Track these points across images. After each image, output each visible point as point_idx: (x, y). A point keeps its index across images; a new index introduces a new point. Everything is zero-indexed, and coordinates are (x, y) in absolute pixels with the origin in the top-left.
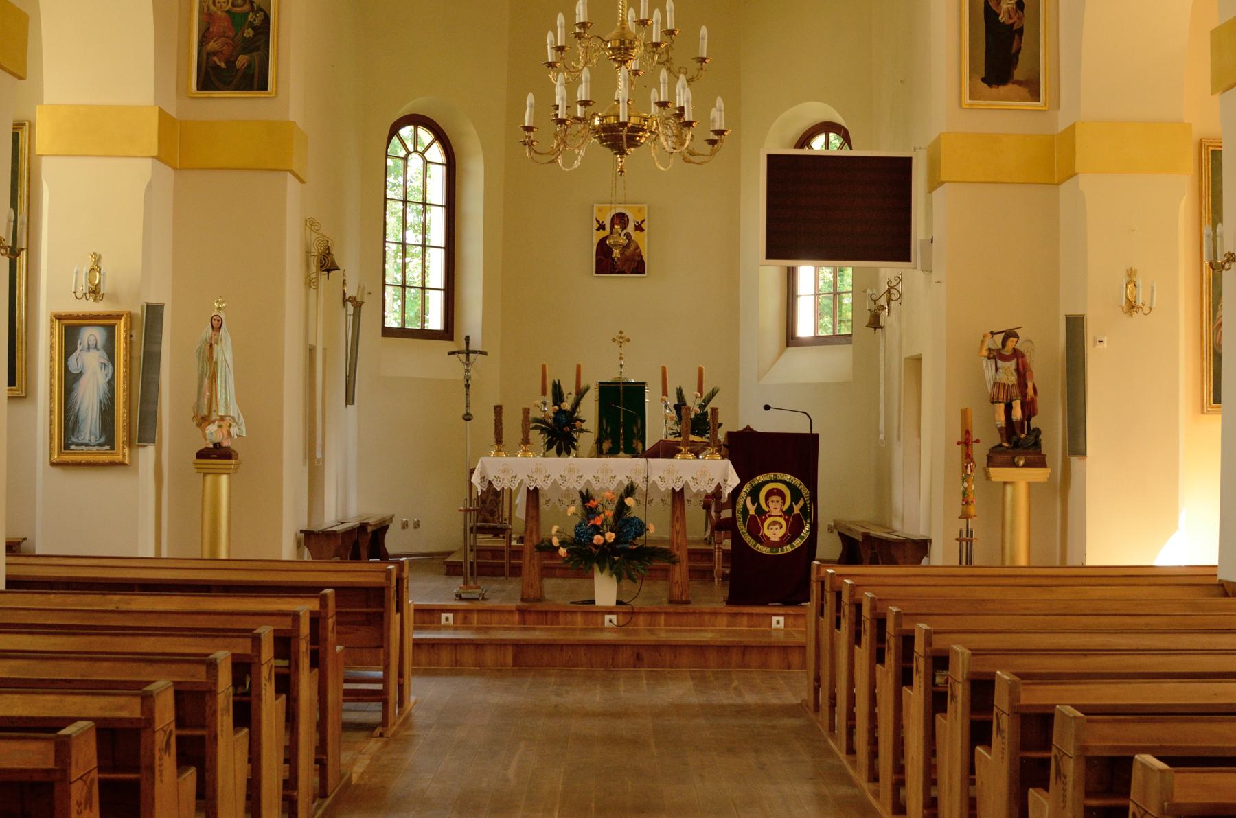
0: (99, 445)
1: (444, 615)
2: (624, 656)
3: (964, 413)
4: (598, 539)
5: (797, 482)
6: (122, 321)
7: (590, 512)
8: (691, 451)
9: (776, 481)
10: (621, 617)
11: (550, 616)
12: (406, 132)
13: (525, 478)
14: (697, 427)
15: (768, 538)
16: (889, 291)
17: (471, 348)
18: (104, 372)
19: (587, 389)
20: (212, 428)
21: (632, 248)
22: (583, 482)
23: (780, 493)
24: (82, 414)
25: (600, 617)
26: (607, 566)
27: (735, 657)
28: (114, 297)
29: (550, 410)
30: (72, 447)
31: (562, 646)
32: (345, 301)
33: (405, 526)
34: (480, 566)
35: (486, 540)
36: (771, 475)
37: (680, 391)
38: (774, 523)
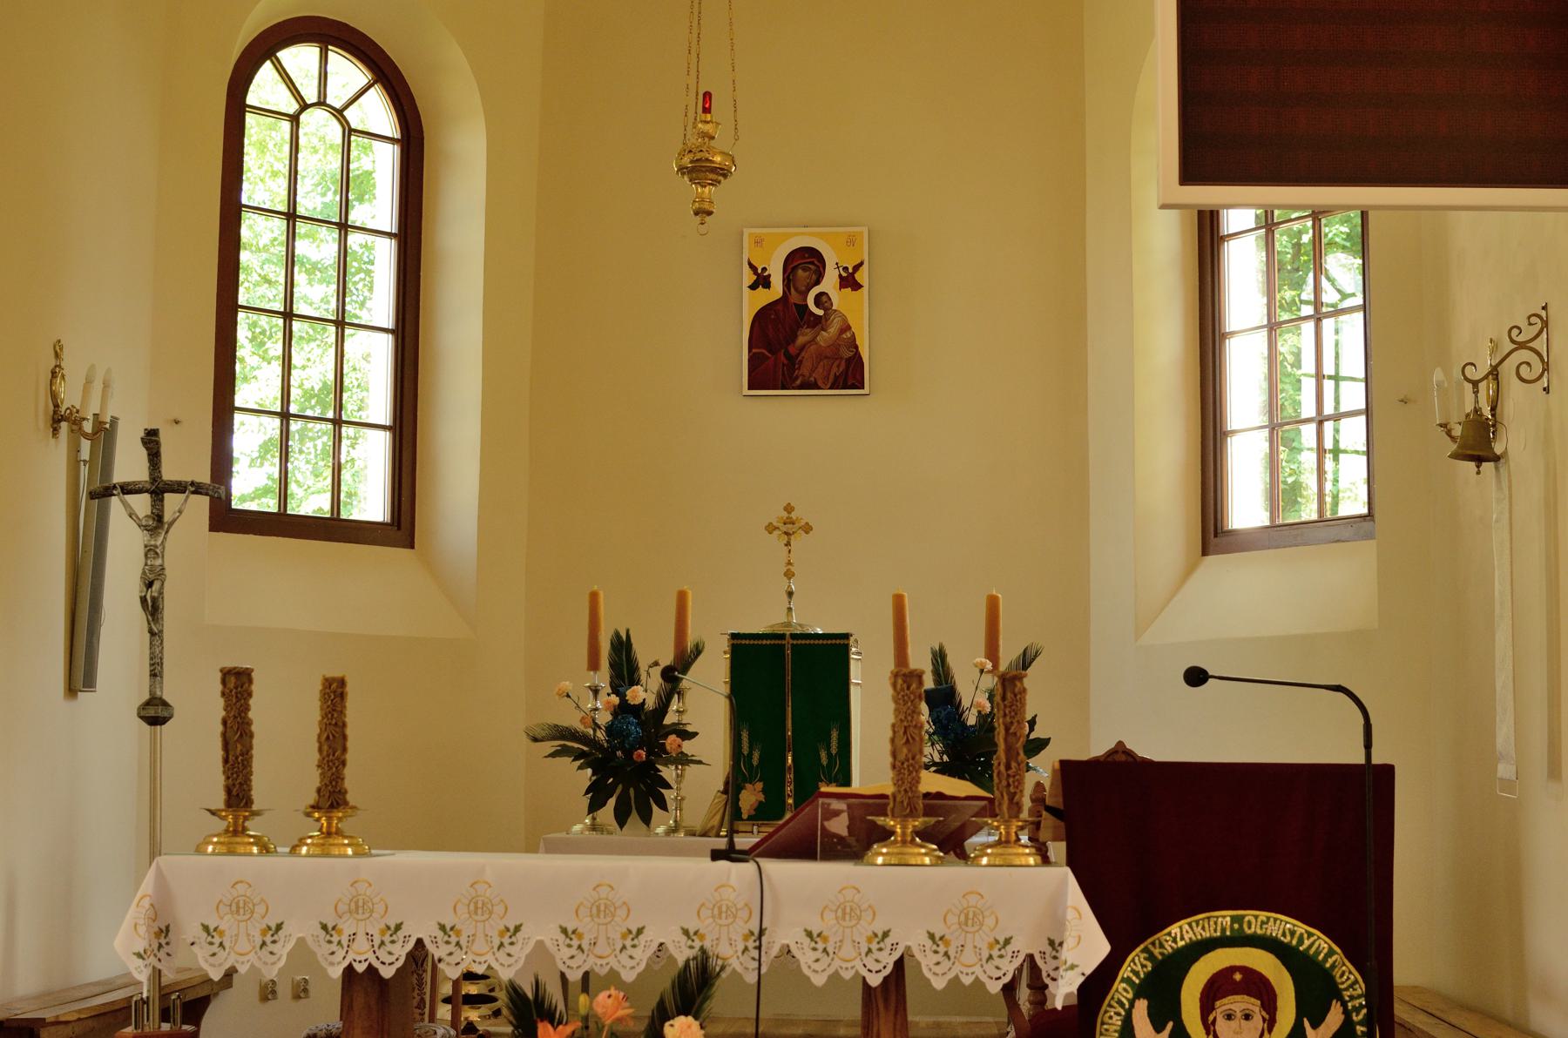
5: (1318, 943)
8: (925, 835)
14: (969, 739)
16: (1494, 373)
17: (169, 473)
19: (698, 651)
21: (833, 330)
29: (603, 708)
32: (56, 420)
33: (268, 992)
36: (1223, 920)
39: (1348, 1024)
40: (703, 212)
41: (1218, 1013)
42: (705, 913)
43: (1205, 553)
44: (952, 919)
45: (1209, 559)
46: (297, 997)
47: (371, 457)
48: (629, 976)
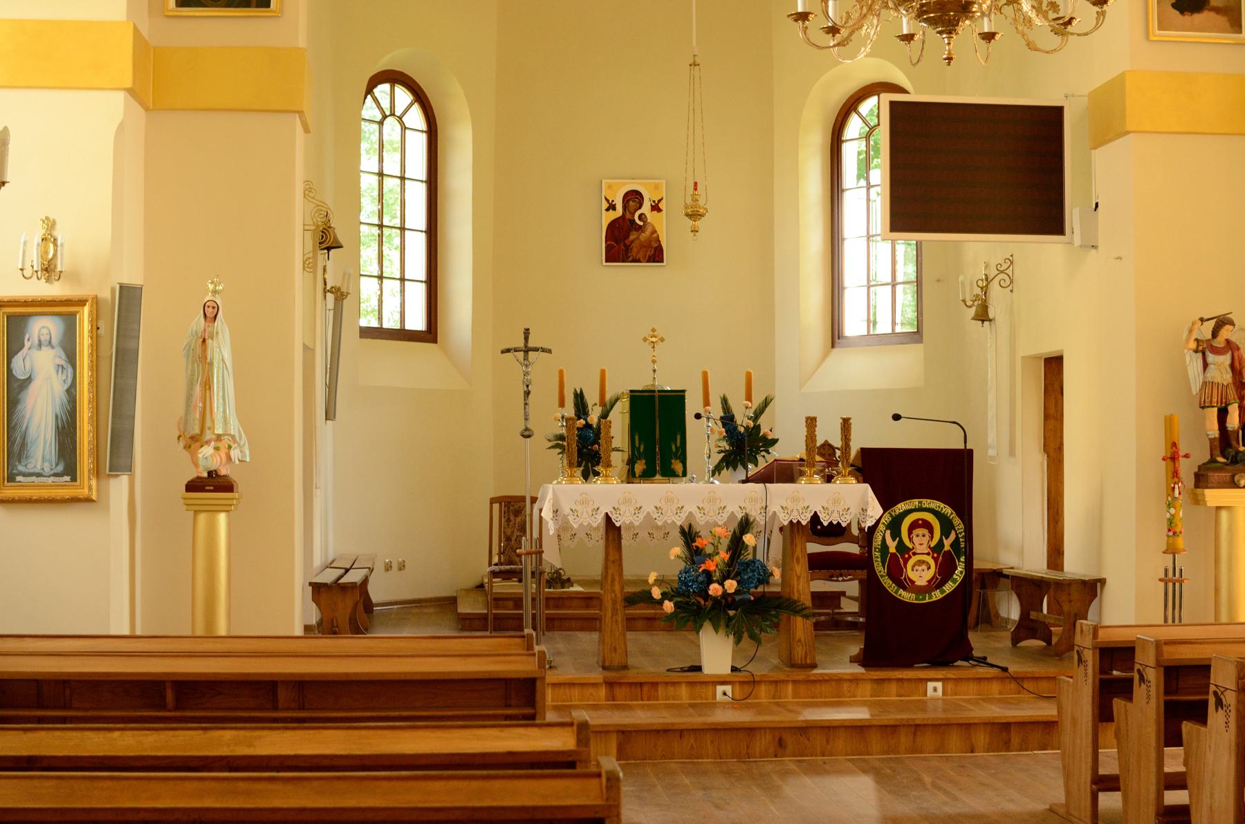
0: (56, 475)
2: (763, 742)
3: (1169, 421)
5: (948, 510)
6: (86, 309)
7: (694, 553)
9: (921, 509)
10: (737, 687)
11: (645, 688)
12: (382, 90)
13: (651, 509)
15: (913, 582)
17: (530, 345)
18: (61, 377)
20: (207, 451)
21: (648, 232)
22: (684, 515)
23: (927, 525)
24: (32, 432)
25: (711, 687)
26: (722, 623)
27: (904, 739)
28: (74, 277)
30: (19, 478)
31: (682, 732)
33: (388, 567)
34: (496, 617)
35: (502, 587)
37: (725, 401)
38: (921, 562)
39: (957, 537)
40: (695, 231)
43: (833, 346)
45: (835, 350)
46: (387, 570)
47: (417, 295)
48: (720, 523)
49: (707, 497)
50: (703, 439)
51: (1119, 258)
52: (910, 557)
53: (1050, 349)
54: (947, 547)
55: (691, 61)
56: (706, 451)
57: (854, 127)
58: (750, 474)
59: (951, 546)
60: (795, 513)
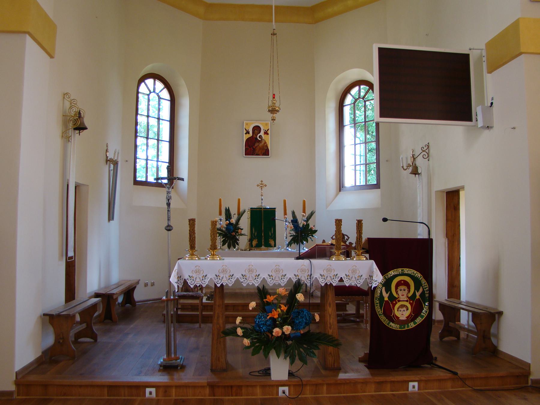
1: (148, 390)
4: (277, 331)
5: (418, 275)
9: (403, 274)
10: (292, 388)
15: (398, 318)
19: (244, 211)
22: (259, 280)
33: (146, 285)
36: (400, 270)
37: (293, 213)
38: (402, 306)
39: (423, 291)
41: (399, 290)
42: (299, 271)
43: (340, 191)
44: (350, 271)
45: (341, 192)
46: (152, 286)
48: (283, 285)
49: (276, 268)
50: (283, 230)
51: (514, 128)
52: (396, 303)
53: (451, 186)
54: (418, 297)
55: (272, 32)
56: (285, 235)
57: (349, 100)
58: (302, 251)
59: (420, 296)
60: (329, 278)
